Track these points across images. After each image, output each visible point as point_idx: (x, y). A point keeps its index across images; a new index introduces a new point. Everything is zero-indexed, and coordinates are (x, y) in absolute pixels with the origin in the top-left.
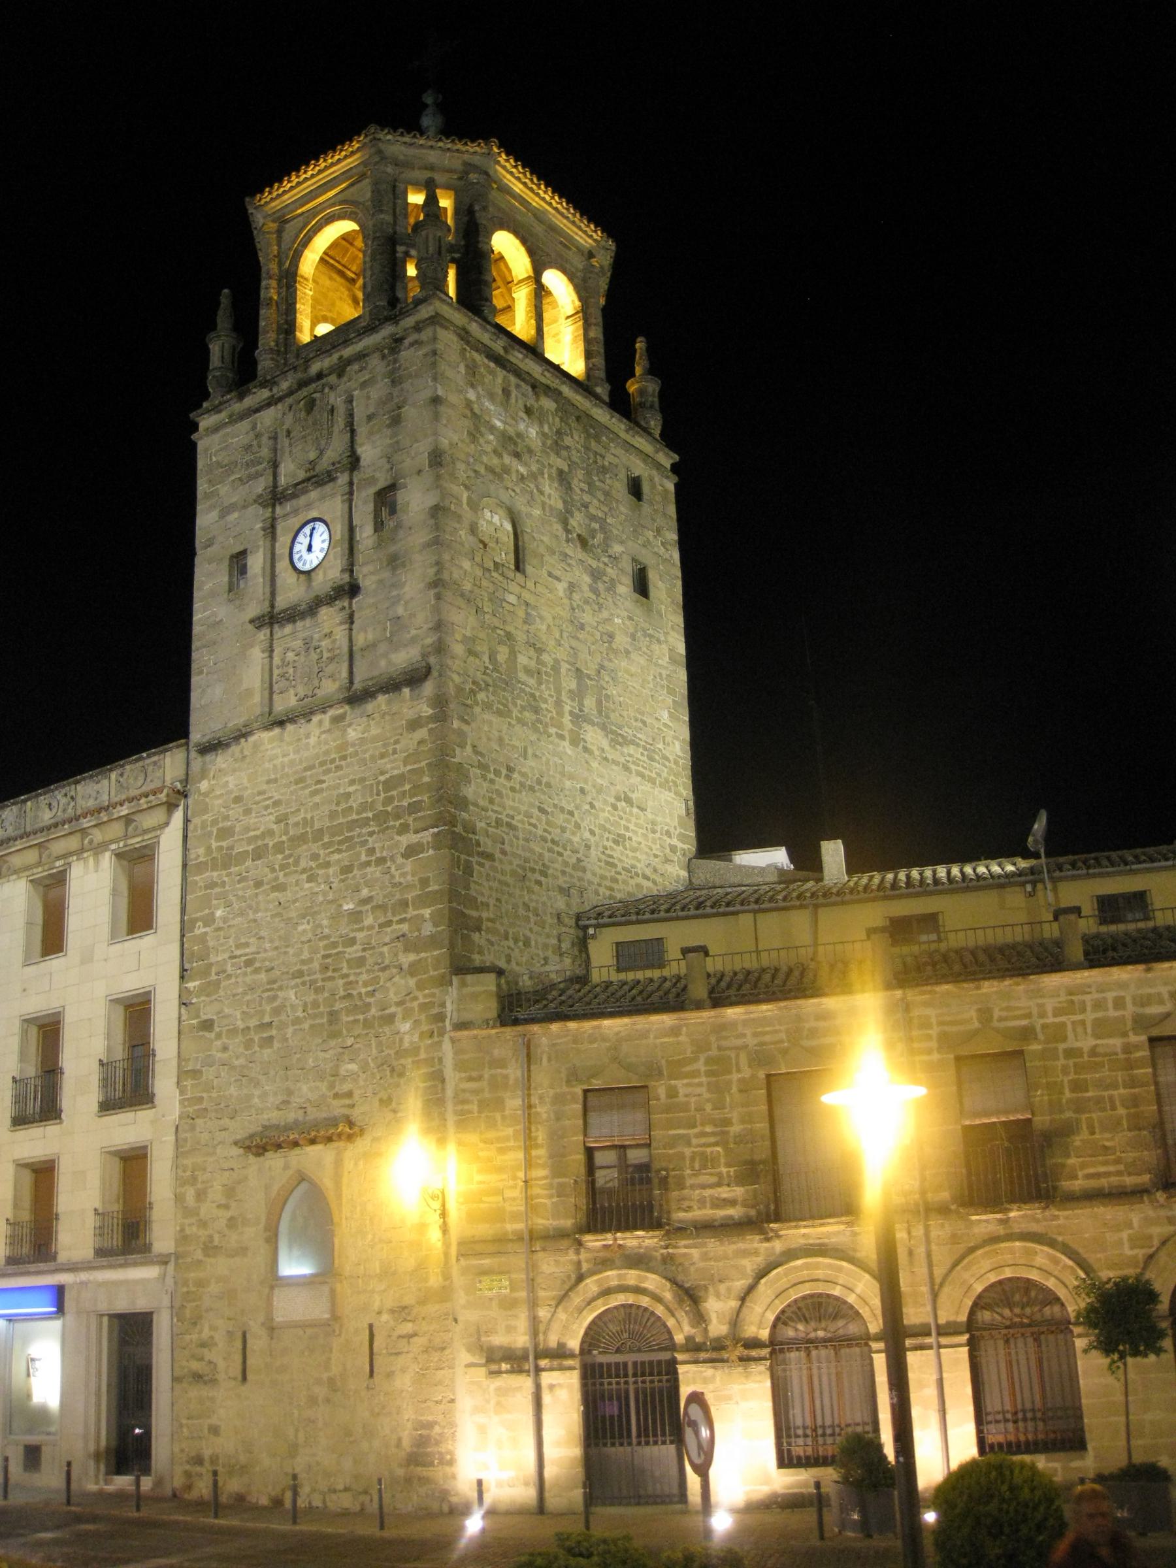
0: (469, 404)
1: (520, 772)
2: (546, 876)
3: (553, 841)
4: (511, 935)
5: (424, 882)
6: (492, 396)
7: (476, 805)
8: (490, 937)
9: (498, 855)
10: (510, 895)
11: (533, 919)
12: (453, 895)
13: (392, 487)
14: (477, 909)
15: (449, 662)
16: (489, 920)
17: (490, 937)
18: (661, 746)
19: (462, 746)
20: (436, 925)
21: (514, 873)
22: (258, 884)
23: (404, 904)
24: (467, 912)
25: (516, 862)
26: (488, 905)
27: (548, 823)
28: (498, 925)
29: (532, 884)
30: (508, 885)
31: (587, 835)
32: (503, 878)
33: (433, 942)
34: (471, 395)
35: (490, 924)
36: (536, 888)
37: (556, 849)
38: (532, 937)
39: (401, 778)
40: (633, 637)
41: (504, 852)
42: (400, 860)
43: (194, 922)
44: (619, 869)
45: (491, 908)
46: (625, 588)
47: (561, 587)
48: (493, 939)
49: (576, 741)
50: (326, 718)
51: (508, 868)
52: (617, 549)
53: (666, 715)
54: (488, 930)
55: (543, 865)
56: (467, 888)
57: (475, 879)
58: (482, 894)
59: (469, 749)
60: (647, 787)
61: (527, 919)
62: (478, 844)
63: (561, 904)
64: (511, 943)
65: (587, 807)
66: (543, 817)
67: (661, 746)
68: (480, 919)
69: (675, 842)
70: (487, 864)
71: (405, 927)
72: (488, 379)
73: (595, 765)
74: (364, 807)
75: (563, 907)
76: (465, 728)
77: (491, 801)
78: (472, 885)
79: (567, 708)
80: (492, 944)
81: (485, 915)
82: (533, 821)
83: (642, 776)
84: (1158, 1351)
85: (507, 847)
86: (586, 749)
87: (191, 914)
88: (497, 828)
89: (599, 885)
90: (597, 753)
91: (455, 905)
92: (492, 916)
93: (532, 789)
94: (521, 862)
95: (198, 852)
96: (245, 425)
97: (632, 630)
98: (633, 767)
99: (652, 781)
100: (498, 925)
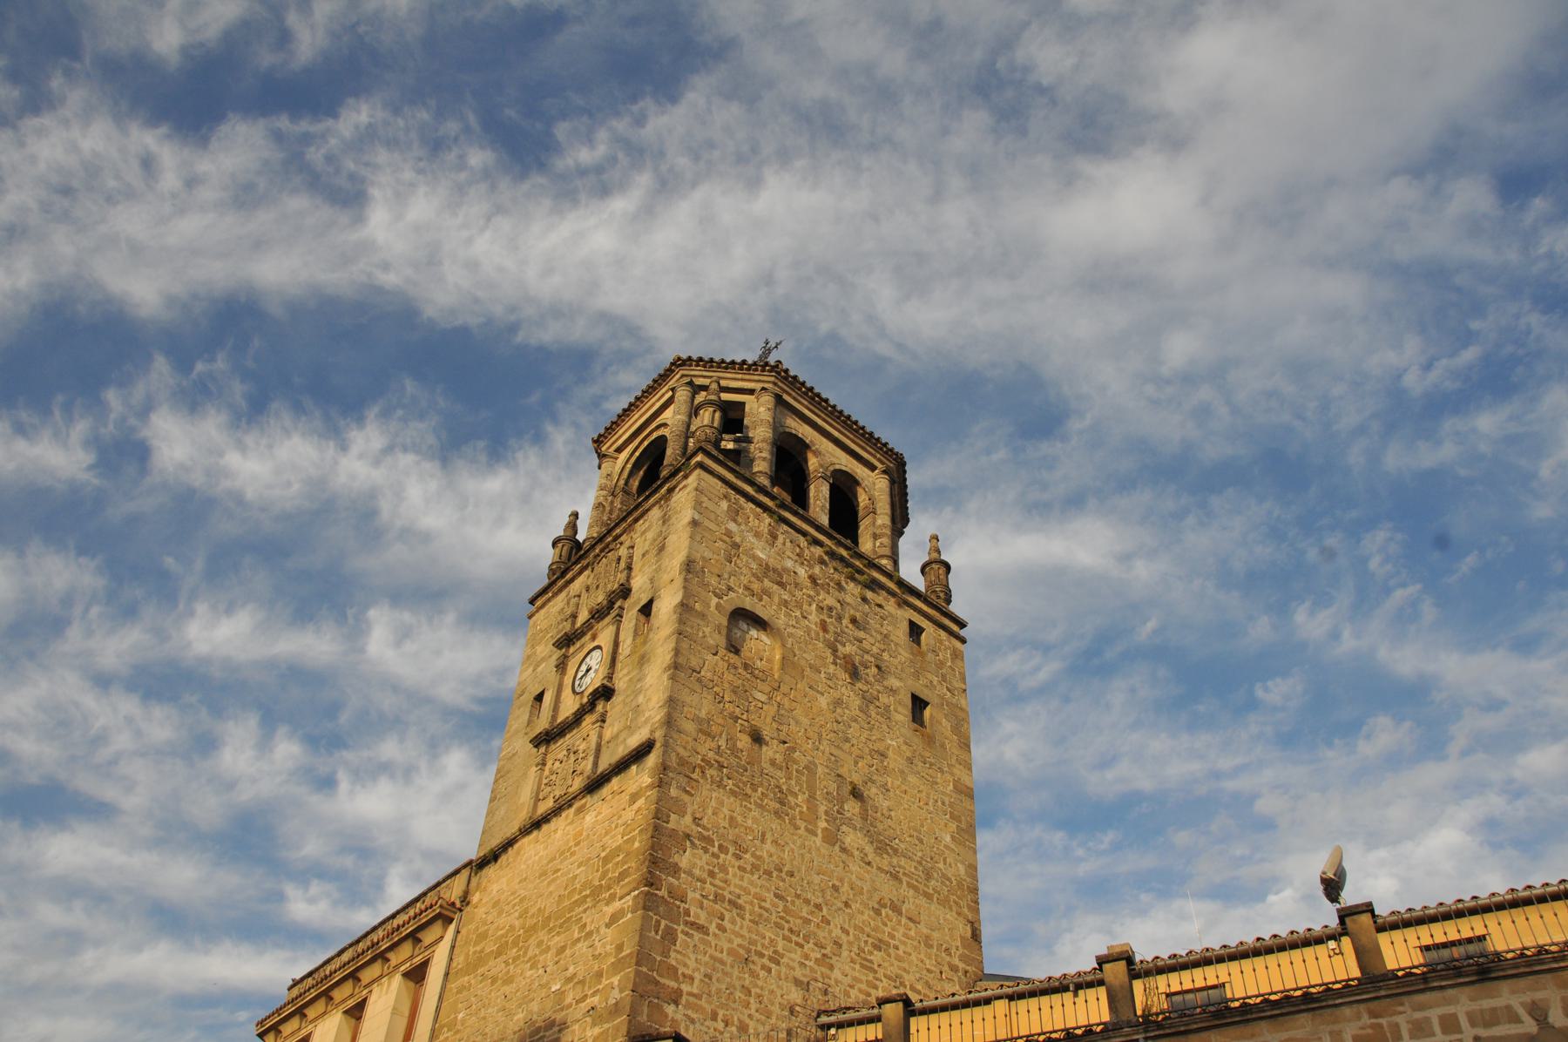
0: (729, 534)
1: (753, 855)
2: (778, 963)
3: (791, 930)
4: (720, 1017)
5: (620, 948)
6: (757, 535)
7: (690, 873)
8: (689, 1012)
9: (713, 928)
10: (726, 974)
11: (754, 1006)
12: (641, 957)
13: (651, 602)
14: (677, 980)
15: (675, 736)
16: (690, 994)
17: (689, 1012)
18: (941, 865)
19: (682, 814)
20: (621, 991)
21: (731, 952)
22: (494, 980)
23: (599, 975)
24: (662, 981)
25: (738, 941)
26: (692, 979)
27: (786, 910)
28: (703, 1003)
29: (757, 968)
30: (722, 963)
31: (837, 932)
32: (718, 955)
33: (616, 1009)
34: (732, 526)
35: (691, 999)
36: (763, 974)
37: (794, 938)
38: (752, 1024)
39: (619, 848)
40: (910, 761)
41: (722, 928)
42: (603, 930)
43: (442, 1027)
44: (880, 975)
45: (697, 982)
46: (902, 715)
47: (823, 702)
48: (694, 1016)
49: (831, 838)
50: (572, 810)
51: (726, 946)
52: (893, 682)
53: (948, 838)
54: (688, 1006)
55: (775, 952)
56: (666, 954)
57: (678, 947)
58: (685, 965)
59: (688, 819)
60: (922, 901)
61: (747, 1006)
62: (687, 913)
63: (795, 995)
64: (721, 1025)
65: (840, 905)
66: (781, 904)
67: (941, 865)
68: (679, 993)
69: (956, 961)
70: (697, 936)
71: (596, 999)
72: (753, 522)
73: (854, 868)
74: (584, 887)
75: (799, 1001)
76: (686, 798)
77: (712, 874)
78: (673, 954)
79: (822, 809)
80: (693, 1021)
81: (685, 988)
82: (767, 905)
83: (916, 889)
84: (1550, 255)
85: (726, 923)
86: (843, 850)
87: (443, 1019)
88: (715, 901)
89: (852, 987)
90: (856, 853)
91: (644, 969)
92: (695, 991)
93: (769, 873)
94: (745, 943)
95: (459, 960)
96: (563, 595)
97: (908, 754)
98: (905, 879)
99: (928, 896)
100: (703, 1003)
